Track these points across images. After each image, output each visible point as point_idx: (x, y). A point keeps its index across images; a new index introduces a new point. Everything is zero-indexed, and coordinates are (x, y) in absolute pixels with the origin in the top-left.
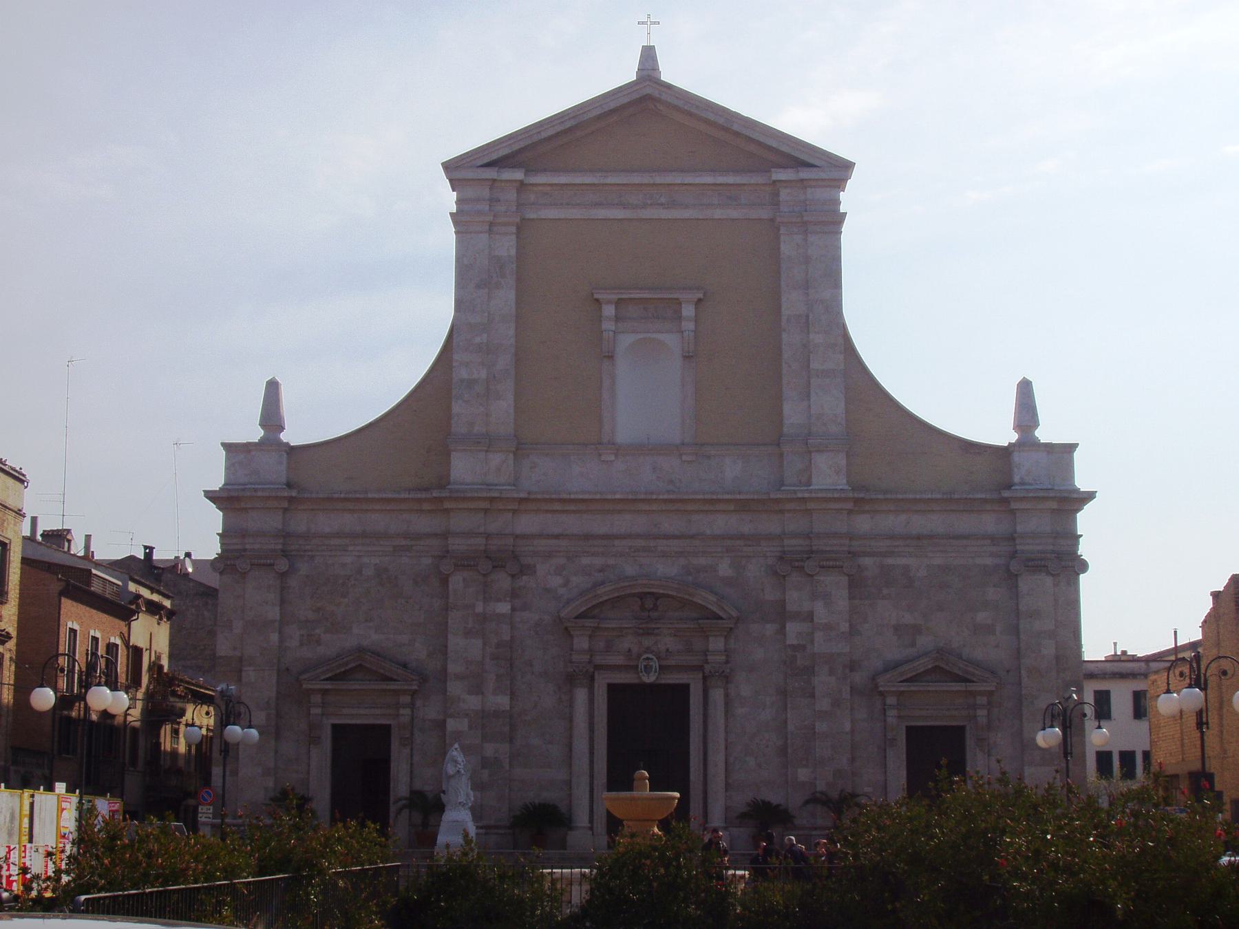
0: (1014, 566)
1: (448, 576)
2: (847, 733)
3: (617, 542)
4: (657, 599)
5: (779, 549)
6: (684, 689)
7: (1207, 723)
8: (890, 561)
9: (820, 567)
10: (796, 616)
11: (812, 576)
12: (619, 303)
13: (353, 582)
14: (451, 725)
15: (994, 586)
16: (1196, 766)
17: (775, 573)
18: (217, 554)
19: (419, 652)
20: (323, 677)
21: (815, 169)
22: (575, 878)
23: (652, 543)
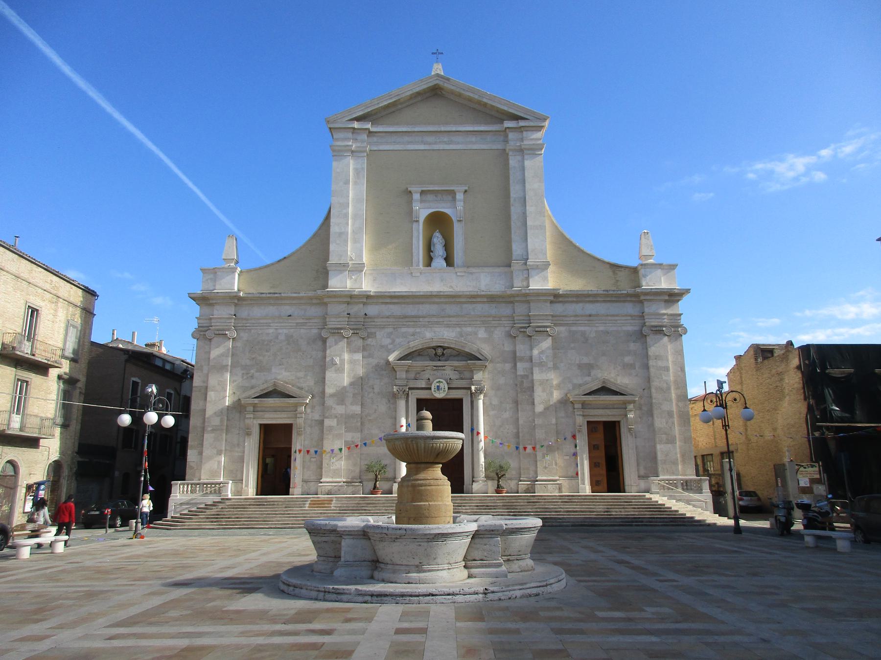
1: (326, 338)
2: (554, 425)
3: (421, 319)
4: (444, 349)
5: (512, 322)
6: (460, 401)
7: (728, 426)
8: (574, 328)
9: (536, 331)
10: (522, 359)
11: (531, 336)
12: (422, 193)
13: (273, 344)
14: (327, 422)
15: (633, 342)
16: (726, 449)
17: (510, 336)
18: (195, 329)
20: (253, 397)
22: (732, 444)
23: (441, 320)
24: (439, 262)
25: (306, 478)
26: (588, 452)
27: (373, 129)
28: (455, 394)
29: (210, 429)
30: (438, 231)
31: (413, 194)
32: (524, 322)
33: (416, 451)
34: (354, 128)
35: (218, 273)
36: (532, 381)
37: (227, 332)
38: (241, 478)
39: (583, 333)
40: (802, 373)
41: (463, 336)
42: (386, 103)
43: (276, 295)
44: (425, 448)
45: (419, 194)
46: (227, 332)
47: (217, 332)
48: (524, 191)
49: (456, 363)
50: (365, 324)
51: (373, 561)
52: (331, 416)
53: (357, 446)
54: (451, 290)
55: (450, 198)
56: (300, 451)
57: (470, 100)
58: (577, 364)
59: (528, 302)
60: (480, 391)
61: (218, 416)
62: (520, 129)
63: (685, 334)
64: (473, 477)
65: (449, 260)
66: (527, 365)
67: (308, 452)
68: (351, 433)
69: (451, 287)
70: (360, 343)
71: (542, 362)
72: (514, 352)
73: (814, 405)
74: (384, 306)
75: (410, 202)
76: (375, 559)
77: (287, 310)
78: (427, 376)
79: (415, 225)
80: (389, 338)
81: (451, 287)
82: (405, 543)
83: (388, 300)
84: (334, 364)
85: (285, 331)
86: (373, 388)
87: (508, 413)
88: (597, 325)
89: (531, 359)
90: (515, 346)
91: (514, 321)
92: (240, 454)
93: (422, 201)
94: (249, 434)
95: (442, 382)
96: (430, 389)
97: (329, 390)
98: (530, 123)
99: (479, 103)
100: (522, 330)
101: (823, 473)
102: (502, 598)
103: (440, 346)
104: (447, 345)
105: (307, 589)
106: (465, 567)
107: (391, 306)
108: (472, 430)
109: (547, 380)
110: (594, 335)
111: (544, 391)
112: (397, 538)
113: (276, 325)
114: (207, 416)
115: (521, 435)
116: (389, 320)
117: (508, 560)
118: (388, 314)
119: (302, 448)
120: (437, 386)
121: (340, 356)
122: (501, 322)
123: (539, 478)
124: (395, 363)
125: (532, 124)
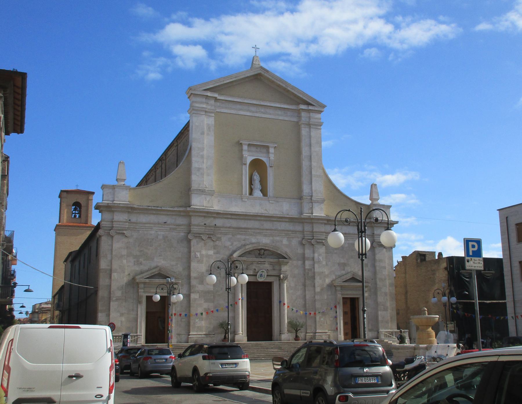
0: (190, 237)
3: (249, 230)
10: (308, 259)
12: (249, 145)
13: (154, 241)
19: (179, 268)
20: (145, 278)
21: (314, 106)
23: (262, 231)
24: (258, 193)
26: (342, 315)
27: (219, 98)
28: (269, 280)
29: (114, 299)
30: (256, 171)
31: (243, 146)
32: (309, 235)
34: (207, 96)
35: (115, 189)
36: (314, 273)
37: (125, 232)
40: (448, 272)
41: (274, 243)
42: (228, 81)
43: (158, 208)
45: (247, 146)
46: (125, 232)
47: (118, 232)
48: (310, 151)
49: (272, 260)
50: (215, 231)
52: (195, 292)
53: (212, 311)
54: (266, 212)
55: (265, 150)
56: (175, 314)
57: (279, 86)
58: (338, 263)
59: (312, 223)
60: (286, 278)
62: (309, 111)
63: (394, 247)
64: (280, 331)
65: (264, 192)
66: (311, 262)
67: (180, 315)
69: (266, 210)
70: (211, 243)
71: (320, 261)
72: (304, 254)
73: (454, 290)
74: (226, 220)
75: (241, 150)
77: (163, 219)
78: (254, 267)
79: (244, 167)
81: (266, 210)
83: (230, 217)
84: (196, 257)
85: (162, 233)
86: (220, 274)
88: (349, 239)
89: (313, 259)
90: (304, 251)
91: (313, 237)
93: (249, 151)
94: (140, 302)
95: (264, 272)
96: (256, 275)
97: (193, 275)
98: (316, 108)
99: (285, 89)
100: (309, 241)
101: (456, 327)
103: (263, 249)
104: (267, 248)
107: (231, 220)
108: (280, 302)
109: (322, 272)
111: (320, 279)
113: (157, 228)
114: (112, 290)
115: (307, 305)
116: (230, 229)
118: (228, 225)
119: (176, 312)
120: (261, 274)
121: (200, 252)
122: (296, 235)
123: (317, 331)
124: (237, 259)
125: (316, 109)
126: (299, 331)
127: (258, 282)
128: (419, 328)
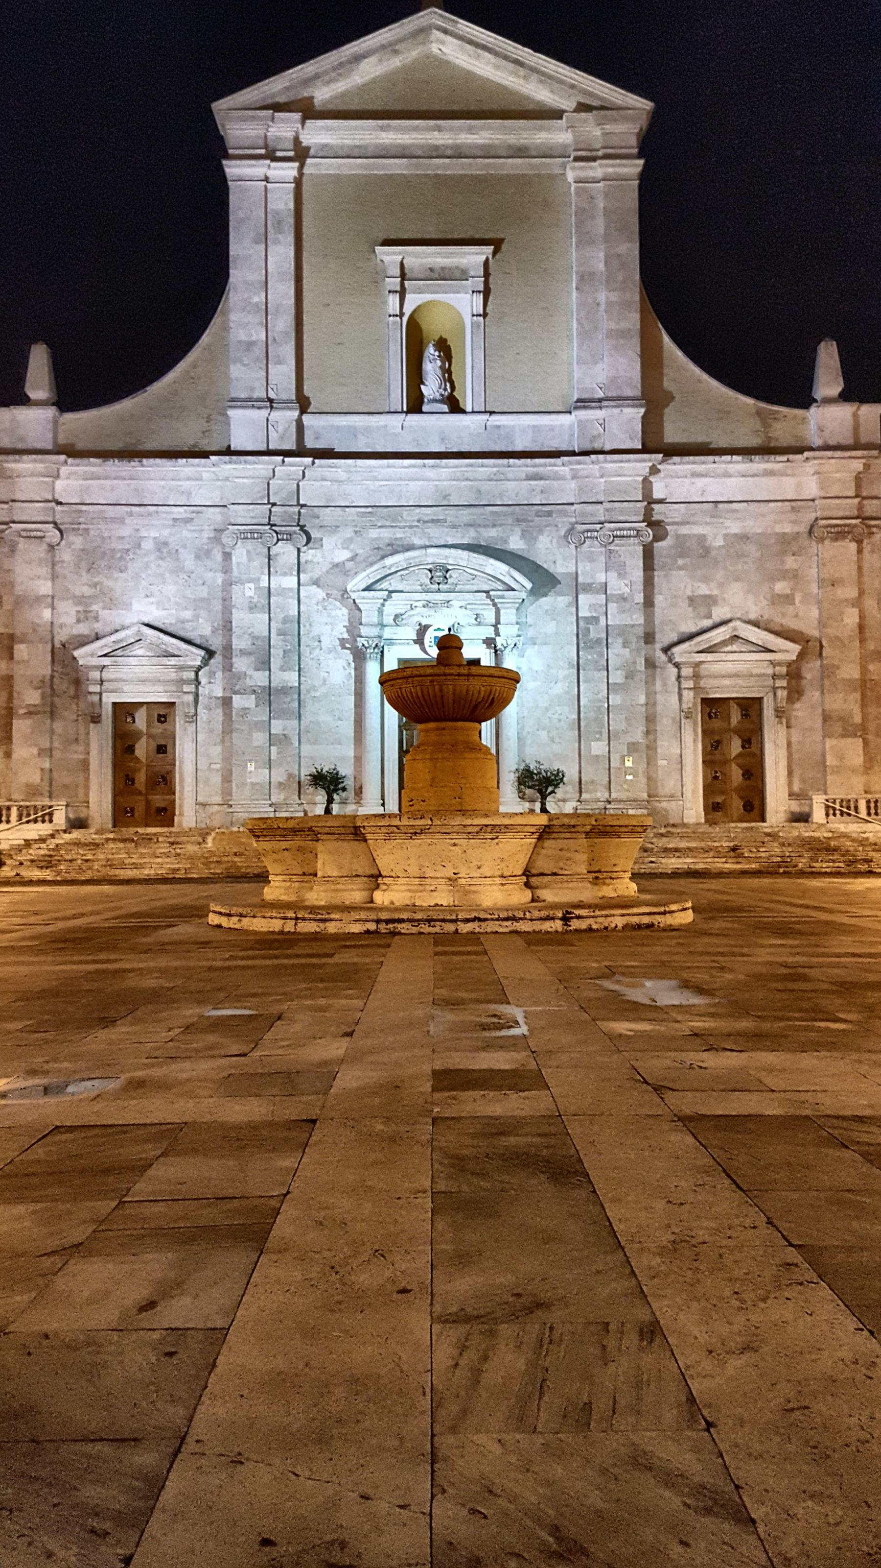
10: (588, 588)
25: (201, 799)
29: (22, 711)
33: (439, 699)
38: (85, 799)
39: (702, 538)
44: (454, 694)
51: (372, 876)
61: (37, 688)
68: (281, 721)
76: (375, 872)
80: (347, 548)
82: (429, 841)
87: (559, 684)
92: (82, 757)
102: (595, 927)
105: (264, 917)
106: (527, 885)
110: (722, 543)
112: (415, 833)
117: (597, 878)
126: (549, 799)
127: (646, 288)
128: (75, 658)
